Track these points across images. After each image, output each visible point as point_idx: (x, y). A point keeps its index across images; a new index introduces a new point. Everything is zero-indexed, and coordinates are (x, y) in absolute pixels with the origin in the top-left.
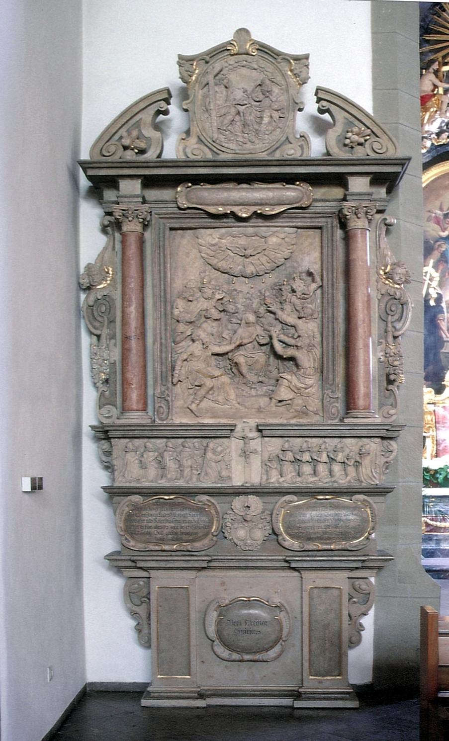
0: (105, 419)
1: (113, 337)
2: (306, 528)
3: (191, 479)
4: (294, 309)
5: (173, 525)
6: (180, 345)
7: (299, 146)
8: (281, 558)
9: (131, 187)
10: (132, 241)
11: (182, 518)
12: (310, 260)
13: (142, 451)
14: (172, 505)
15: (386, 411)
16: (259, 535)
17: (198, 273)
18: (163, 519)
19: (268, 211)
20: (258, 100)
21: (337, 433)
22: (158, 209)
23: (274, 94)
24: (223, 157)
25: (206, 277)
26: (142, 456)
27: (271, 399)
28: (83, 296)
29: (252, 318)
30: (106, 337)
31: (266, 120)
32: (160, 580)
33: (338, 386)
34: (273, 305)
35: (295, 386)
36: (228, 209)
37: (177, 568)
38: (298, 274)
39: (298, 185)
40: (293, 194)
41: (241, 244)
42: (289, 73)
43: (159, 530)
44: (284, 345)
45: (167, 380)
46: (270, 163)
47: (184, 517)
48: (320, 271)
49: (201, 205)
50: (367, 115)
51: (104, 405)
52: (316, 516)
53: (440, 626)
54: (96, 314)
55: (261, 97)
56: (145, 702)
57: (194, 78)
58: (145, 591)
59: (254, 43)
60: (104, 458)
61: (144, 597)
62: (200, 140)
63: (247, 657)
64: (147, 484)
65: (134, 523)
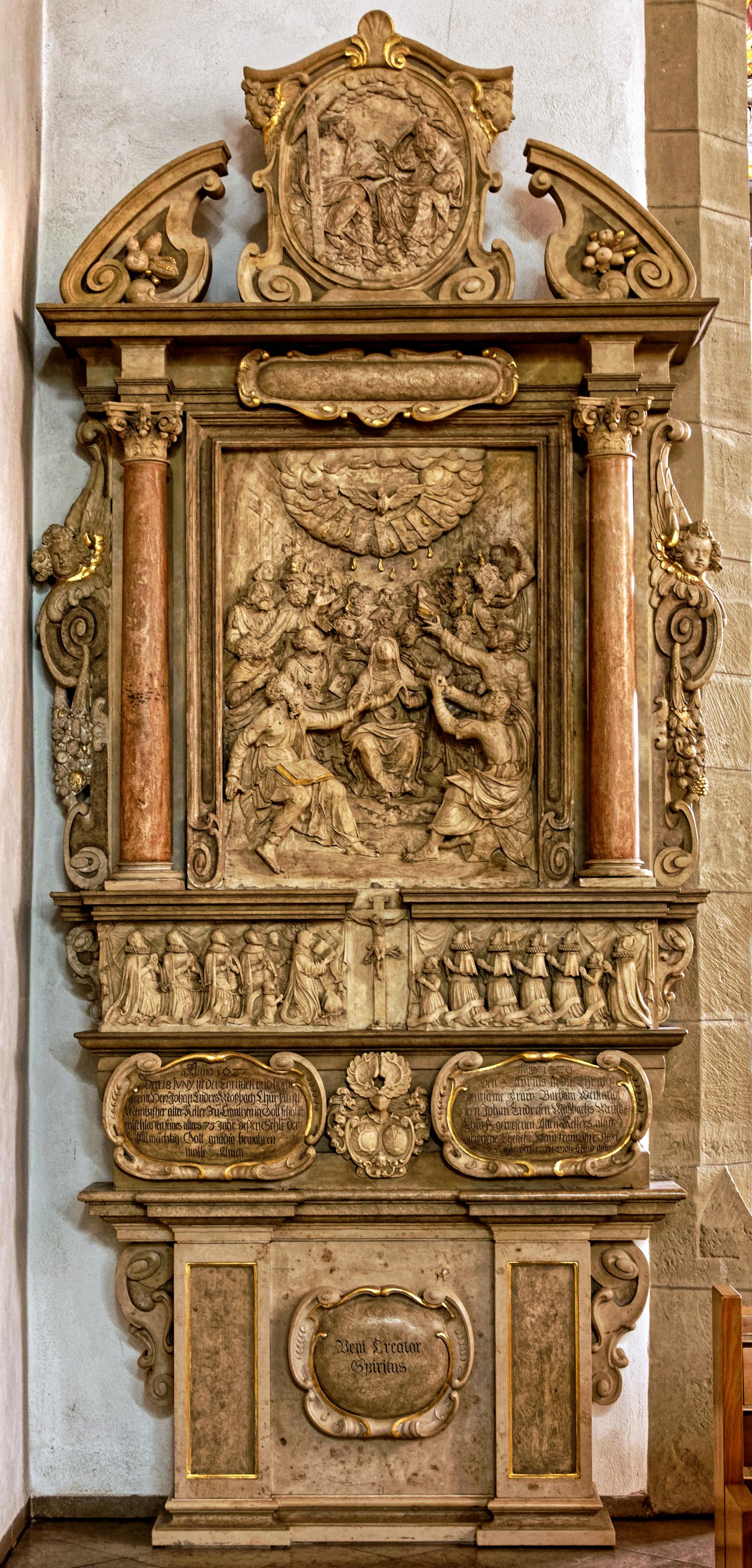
0: (81, 877)
1: (101, 691)
2: (500, 1126)
3: (262, 1014)
4: (478, 630)
5: (223, 1120)
6: (242, 710)
7: (491, 271)
8: (448, 1194)
9: (144, 363)
10: (150, 484)
11: (244, 1106)
12: (512, 518)
13: (160, 952)
14: (224, 1076)
15: (672, 857)
16: (401, 1141)
17: (280, 546)
18: (204, 1106)
19: (424, 411)
20: (406, 167)
21: (567, 911)
22: (199, 407)
23: (440, 157)
24: (334, 297)
25: (297, 558)
26: (161, 963)
27: (429, 832)
28: (38, 598)
29: (390, 650)
30: (87, 691)
31: (424, 214)
32: (195, 1249)
33: (569, 803)
34: (435, 621)
35: (480, 804)
36: (344, 408)
37: (231, 1221)
38: (488, 550)
39: (489, 356)
40: (476, 376)
41: (368, 484)
42: (472, 108)
43: (194, 1133)
44: (457, 710)
45: (213, 792)
46: (431, 313)
47: (248, 1102)
48: (532, 543)
49: (289, 399)
50: (631, 204)
51: (81, 846)
52: (520, 1099)
53: (745, 1325)
54: (65, 639)
55: (414, 162)
56: (160, 1537)
57: (275, 119)
58: (162, 1279)
59: (403, 42)
60: (78, 968)
61: (159, 1289)
62: (287, 259)
63: (375, 1427)
64: (167, 1028)
65: (144, 1117)
